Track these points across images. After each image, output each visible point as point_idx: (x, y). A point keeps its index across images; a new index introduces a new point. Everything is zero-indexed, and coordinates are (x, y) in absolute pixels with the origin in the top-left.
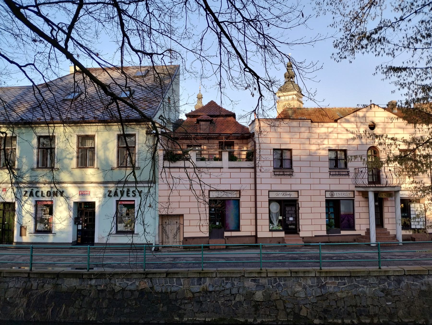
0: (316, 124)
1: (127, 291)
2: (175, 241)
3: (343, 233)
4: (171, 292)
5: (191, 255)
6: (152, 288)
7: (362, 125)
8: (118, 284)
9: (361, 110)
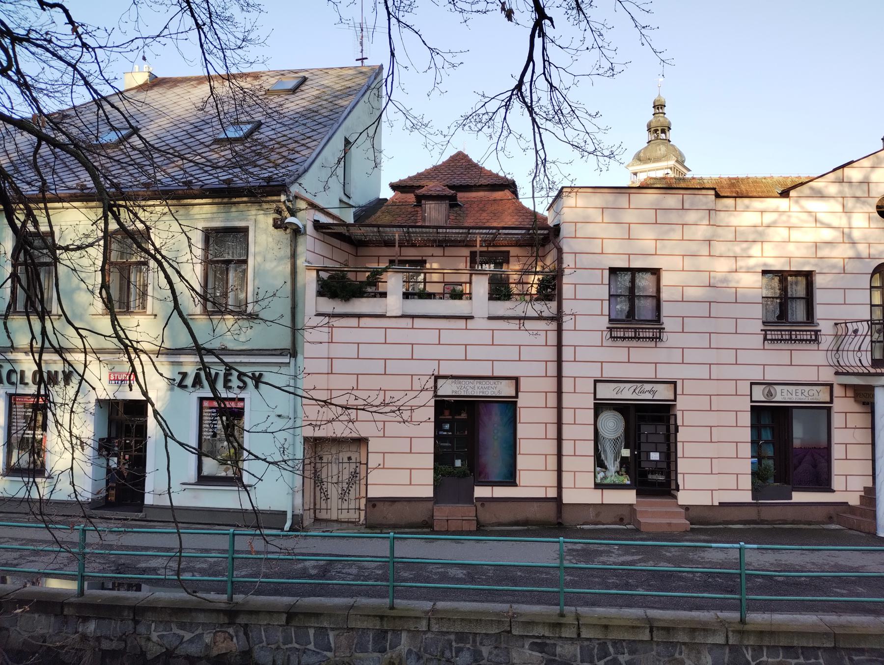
0: (730, 202)
1: (178, 657)
2: (345, 506)
3: (798, 497)
5: (376, 547)
7: (858, 205)
9: (854, 165)
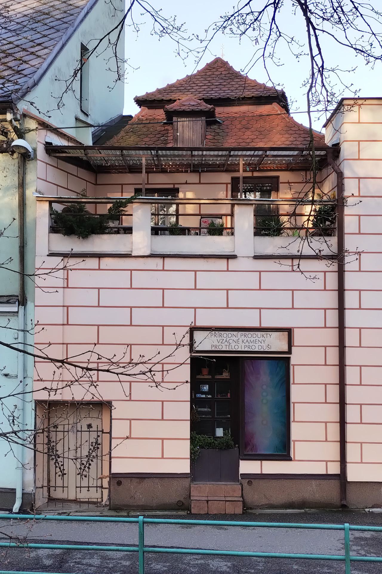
5: (122, 533)
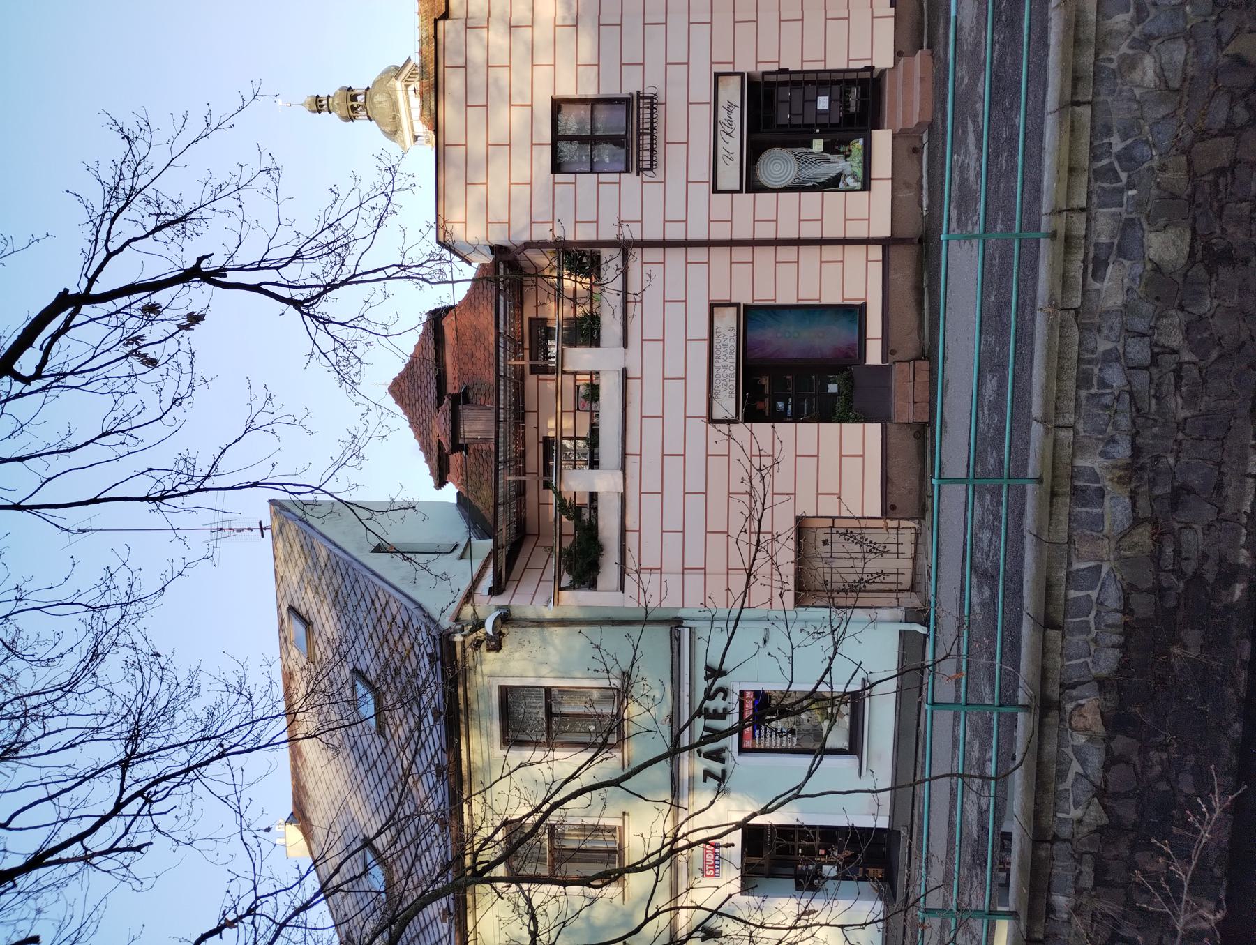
1: (1106, 781)
2: (893, 548)
4: (1126, 609)
6: (1102, 685)
8: (1077, 812)
